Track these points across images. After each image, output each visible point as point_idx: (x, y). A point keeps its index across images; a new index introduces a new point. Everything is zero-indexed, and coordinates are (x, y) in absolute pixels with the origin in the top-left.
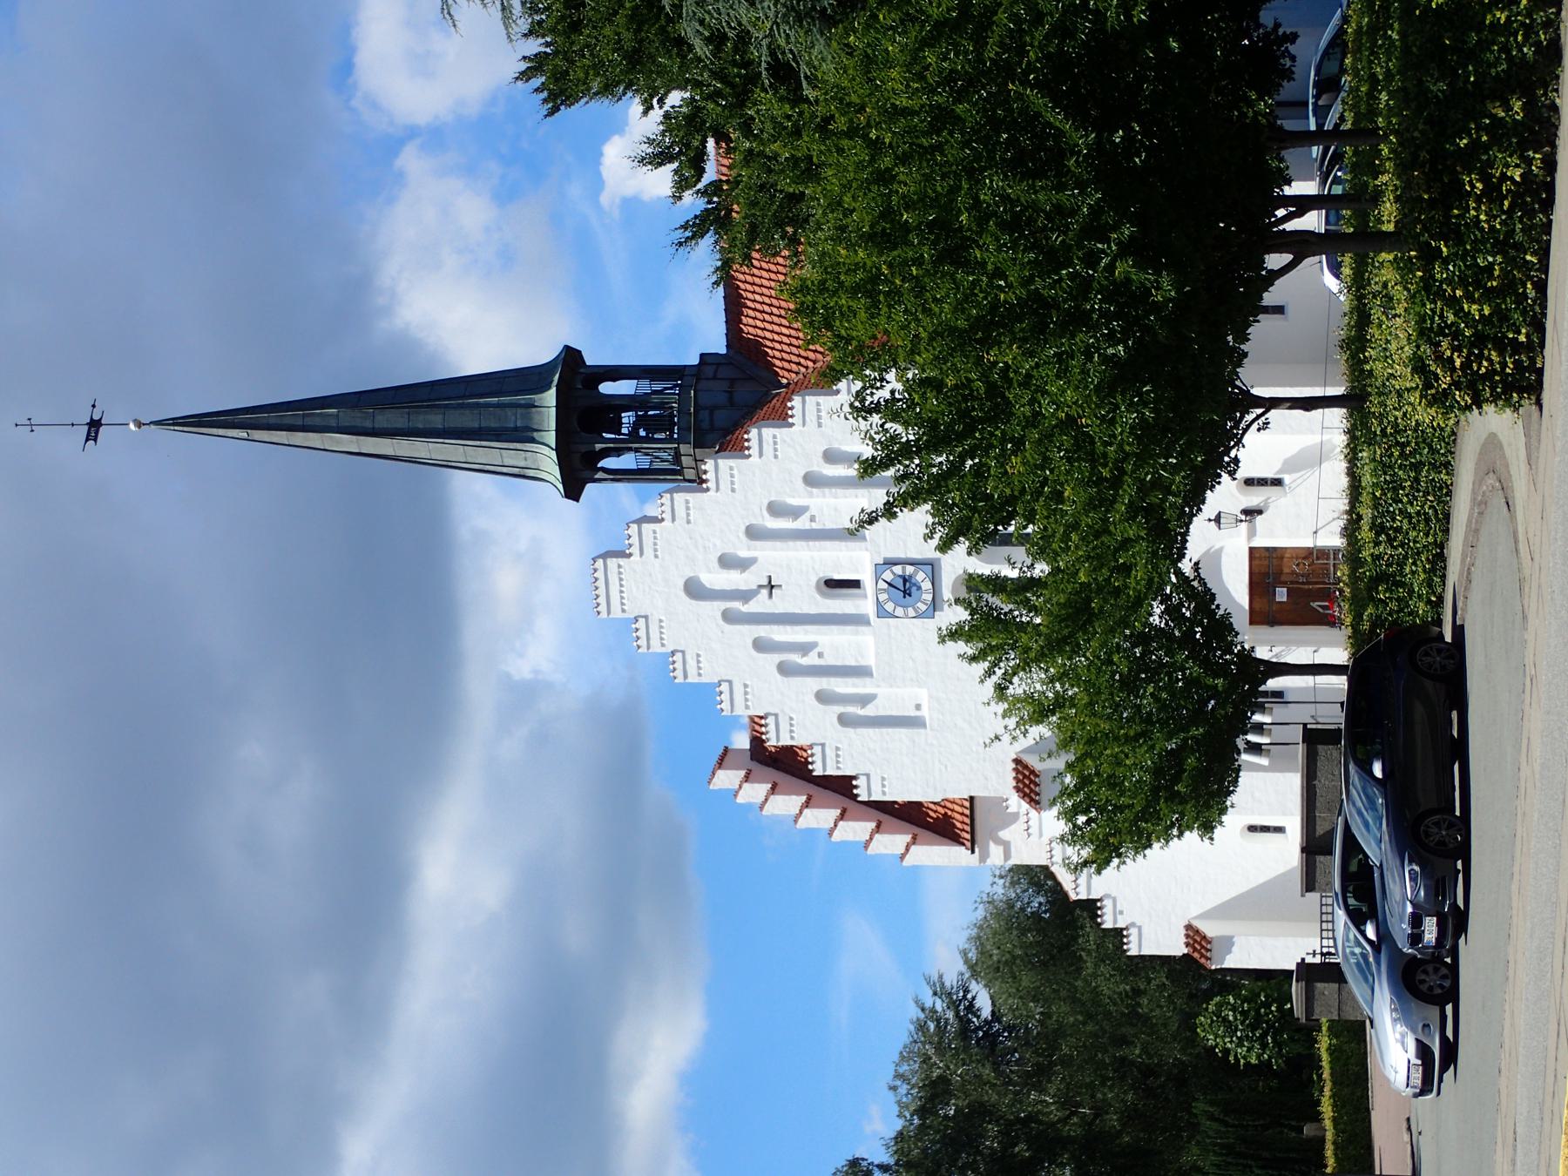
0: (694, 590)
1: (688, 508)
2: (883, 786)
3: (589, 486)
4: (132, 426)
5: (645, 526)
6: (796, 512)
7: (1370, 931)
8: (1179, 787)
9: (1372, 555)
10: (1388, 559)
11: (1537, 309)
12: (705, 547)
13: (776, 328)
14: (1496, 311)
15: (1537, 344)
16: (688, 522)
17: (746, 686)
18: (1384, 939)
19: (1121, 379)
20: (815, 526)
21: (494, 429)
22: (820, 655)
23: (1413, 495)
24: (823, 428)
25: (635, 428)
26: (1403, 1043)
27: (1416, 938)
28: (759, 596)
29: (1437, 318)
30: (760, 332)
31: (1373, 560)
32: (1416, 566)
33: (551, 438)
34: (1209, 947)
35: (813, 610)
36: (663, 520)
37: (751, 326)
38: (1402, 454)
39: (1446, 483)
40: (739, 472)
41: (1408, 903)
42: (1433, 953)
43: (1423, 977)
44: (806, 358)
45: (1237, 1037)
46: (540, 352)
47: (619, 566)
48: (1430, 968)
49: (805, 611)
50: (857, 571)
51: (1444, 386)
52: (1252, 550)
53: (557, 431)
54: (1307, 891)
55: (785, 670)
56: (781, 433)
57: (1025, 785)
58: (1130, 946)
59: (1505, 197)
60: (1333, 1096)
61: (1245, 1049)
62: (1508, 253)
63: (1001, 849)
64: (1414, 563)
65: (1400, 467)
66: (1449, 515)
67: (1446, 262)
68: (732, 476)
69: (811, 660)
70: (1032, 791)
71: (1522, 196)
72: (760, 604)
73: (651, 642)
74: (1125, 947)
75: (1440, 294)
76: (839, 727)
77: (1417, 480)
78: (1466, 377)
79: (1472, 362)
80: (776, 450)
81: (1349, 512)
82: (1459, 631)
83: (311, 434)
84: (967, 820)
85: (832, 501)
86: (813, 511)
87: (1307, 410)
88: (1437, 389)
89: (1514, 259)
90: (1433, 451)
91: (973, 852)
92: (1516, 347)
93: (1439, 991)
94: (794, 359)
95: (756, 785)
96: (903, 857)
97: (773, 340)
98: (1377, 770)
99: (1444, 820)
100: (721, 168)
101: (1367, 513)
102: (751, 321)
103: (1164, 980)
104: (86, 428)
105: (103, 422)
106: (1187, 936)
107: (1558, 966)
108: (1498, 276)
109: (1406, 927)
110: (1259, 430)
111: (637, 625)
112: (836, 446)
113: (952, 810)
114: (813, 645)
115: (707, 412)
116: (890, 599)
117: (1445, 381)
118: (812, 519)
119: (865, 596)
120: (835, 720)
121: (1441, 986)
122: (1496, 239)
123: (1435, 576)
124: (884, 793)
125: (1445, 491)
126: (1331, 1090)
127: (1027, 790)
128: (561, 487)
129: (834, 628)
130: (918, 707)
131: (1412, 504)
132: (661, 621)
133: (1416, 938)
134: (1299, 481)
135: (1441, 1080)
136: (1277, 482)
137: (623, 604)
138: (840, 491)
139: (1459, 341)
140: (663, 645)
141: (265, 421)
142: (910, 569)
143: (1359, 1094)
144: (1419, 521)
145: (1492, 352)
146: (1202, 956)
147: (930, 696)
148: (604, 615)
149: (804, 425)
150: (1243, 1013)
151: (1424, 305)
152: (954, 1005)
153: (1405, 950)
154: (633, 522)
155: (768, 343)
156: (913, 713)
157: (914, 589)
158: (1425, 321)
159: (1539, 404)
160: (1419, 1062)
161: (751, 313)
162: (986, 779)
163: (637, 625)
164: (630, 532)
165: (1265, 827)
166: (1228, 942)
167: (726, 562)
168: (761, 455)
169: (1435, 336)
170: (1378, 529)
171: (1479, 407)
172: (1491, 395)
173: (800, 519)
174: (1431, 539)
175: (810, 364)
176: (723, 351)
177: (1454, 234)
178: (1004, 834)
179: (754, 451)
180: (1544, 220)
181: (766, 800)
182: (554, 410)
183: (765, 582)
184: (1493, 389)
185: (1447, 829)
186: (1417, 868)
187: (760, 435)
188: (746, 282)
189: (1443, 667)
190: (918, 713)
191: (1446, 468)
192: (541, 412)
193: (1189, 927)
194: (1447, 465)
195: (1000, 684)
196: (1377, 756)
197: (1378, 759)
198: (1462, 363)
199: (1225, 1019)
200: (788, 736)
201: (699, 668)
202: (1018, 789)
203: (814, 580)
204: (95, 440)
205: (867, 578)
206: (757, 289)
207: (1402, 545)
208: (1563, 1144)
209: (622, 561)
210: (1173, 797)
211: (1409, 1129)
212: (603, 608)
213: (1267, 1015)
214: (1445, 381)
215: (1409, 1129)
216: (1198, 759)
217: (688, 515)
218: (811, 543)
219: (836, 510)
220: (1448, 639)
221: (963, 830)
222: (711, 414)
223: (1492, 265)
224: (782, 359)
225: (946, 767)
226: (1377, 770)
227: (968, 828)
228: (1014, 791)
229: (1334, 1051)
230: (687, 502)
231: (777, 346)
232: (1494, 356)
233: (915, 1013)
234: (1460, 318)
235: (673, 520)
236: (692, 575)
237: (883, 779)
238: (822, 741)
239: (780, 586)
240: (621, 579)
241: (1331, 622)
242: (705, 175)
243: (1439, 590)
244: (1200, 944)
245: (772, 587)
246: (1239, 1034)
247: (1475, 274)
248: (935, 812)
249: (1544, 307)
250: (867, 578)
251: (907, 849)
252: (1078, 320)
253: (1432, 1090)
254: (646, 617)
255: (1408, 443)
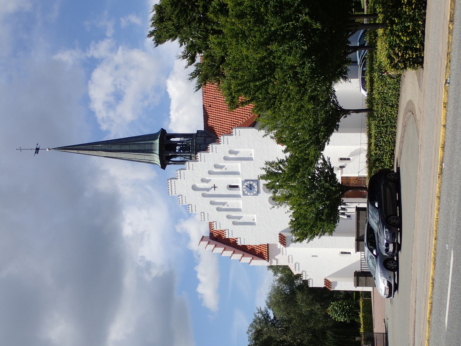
0: (195, 188)
1: (193, 166)
2: (244, 241)
3: (167, 165)
4: (47, 150)
5: (181, 171)
6: (221, 167)
7: (375, 252)
8: (323, 217)
9: (374, 153)
10: (379, 154)
11: (422, 39)
12: (197, 177)
13: (217, 123)
14: (411, 39)
15: (422, 50)
16: (193, 170)
17: (208, 214)
18: (379, 254)
19: (306, 55)
20: (226, 171)
21: (143, 150)
22: (228, 206)
23: (386, 136)
24: (229, 145)
25: (180, 150)
26: (384, 282)
27: (387, 250)
28: (212, 190)
29: (394, 42)
30: (213, 124)
31: (375, 155)
32: (386, 157)
33: (157, 152)
34: (331, 284)
35: (226, 194)
36: (186, 169)
37: (210, 123)
38: (383, 123)
39: (394, 132)
40: (206, 156)
41: (385, 240)
42: (392, 255)
43: (389, 264)
44: (225, 131)
45: (338, 314)
46: (156, 130)
47: (175, 182)
48: (391, 262)
49: (224, 194)
50: (237, 183)
51: (396, 62)
52: (342, 177)
53: (159, 150)
54: (357, 286)
55: (218, 209)
56: (218, 146)
57: (282, 240)
58: (310, 285)
59: (413, 4)
60: (364, 328)
61: (340, 317)
62: (414, 22)
63: (276, 261)
64: (386, 156)
65: (382, 127)
66: (395, 141)
67: (396, 25)
68: (205, 157)
69: (225, 207)
70: (284, 242)
71: (418, 5)
72: (212, 192)
73: (183, 202)
74: (308, 285)
75: (395, 34)
76: (233, 225)
77: (387, 131)
78: (402, 59)
79: (404, 55)
80: (216, 150)
81: (369, 143)
82: (398, 169)
83: (94, 152)
84: (267, 253)
85: (231, 164)
86: (226, 167)
87: (357, 113)
88: (394, 63)
89: (416, 24)
90: (391, 122)
91: (268, 262)
92: (416, 50)
93: (393, 268)
94: (222, 131)
95: (211, 245)
96: (249, 263)
97: (216, 126)
98: (376, 205)
99: (395, 218)
100: (204, 97)
101: (373, 141)
102: (210, 122)
103: (319, 306)
104: (35, 150)
105: (40, 149)
106: (325, 282)
107: (430, 214)
108: (411, 29)
109: (384, 247)
110: (344, 118)
111: (179, 198)
112: (232, 149)
113: (263, 251)
114: (226, 203)
115: (199, 145)
116: (246, 190)
117: (396, 60)
118: (226, 169)
119: (240, 190)
120: (232, 223)
121: (394, 267)
122: (411, 18)
123: (392, 159)
124: (244, 243)
125: (394, 134)
126: (363, 327)
127: (282, 242)
128: (160, 165)
129: (232, 198)
130: (254, 220)
131: (385, 138)
132: (185, 196)
133: (387, 250)
134: (355, 158)
135: (394, 294)
136: (349, 159)
137: (175, 192)
138: (233, 161)
139: (400, 49)
140: (186, 203)
141: (82, 148)
142: (252, 182)
143: (371, 327)
144: (387, 143)
145: (410, 51)
146: (329, 287)
147: (257, 217)
148: (170, 195)
149: (224, 143)
150: (339, 307)
151: (390, 38)
152: (263, 315)
153: (384, 254)
154: (178, 170)
155: (215, 127)
156: (252, 221)
157: (253, 188)
158: (391, 43)
159: (423, 67)
160: (388, 287)
161: (210, 119)
162: (272, 239)
163: (179, 198)
164: (177, 172)
165: (345, 252)
166: (336, 283)
167: (203, 181)
168: (212, 152)
169: (394, 48)
170: (376, 145)
171: (406, 69)
172: (409, 65)
173: (223, 169)
174: (390, 148)
175: (226, 132)
176: (203, 130)
177: (399, 16)
178: (276, 257)
179: (211, 151)
180: (424, 12)
181: (214, 249)
182: (158, 145)
183: (213, 186)
184: (410, 63)
185: (395, 220)
186: (387, 230)
187: (212, 146)
188: (209, 111)
189: (394, 179)
190: (254, 221)
191: (394, 127)
192: (154, 145)
193: (325, 279)
194: (395, 126)
195: (274, 192)
196: (376, 201)
197: (377, 202)
198: (401, 55)
199: (335, 309)
200: (219, 228)
201: (196, 209)
202: (280, 242)
203: (226, 185)
204: (38, 153)
205: (240, 185)
206: (212, 113)
207: (383, 150)
208: (432, 264)
209: (175, 180)
210: (321, 220)
211: (385, 322)
212: (170, 193)
213: (346, 308)
214: (396, 60)
215: (385, 322)
216: (328, 210)
217: (193, 168)
218: (225, 175)
219: (232, 167)
220: (395, 171)
221: (266, 256)
222: (200, 146)
223: (409, 26)
224: (219, 131)
225: (261, 236)
226: (376, 205)
227: (267, 255)
228: (279, 242)
229: (364, 316)
230: (193, 164)
231: (217, 128)
232: (410, 53)
233: (254, 317)
234: (400, 42)
235: (189, 169)
236: (194, 184)
237: (244, 239)
238: (228, 229)
239: (217, 187)
240: (175, 185)
241: (364, 197)
242: (196, 62)
243: (393, 163)
244: (328, 284)
245: (215, 187)
246: (339, 313)
247: (405, 29)
248: (258, 251)
249: (424, 39)
250: (240, 185)
251: (251, 261)
252: (293, 37)
253: (391, 296)
254: (182, 195)
255: (384, 120)
